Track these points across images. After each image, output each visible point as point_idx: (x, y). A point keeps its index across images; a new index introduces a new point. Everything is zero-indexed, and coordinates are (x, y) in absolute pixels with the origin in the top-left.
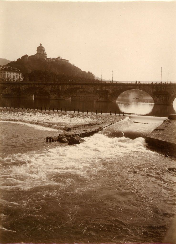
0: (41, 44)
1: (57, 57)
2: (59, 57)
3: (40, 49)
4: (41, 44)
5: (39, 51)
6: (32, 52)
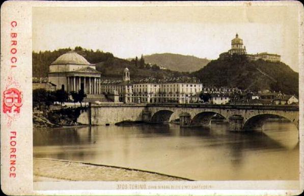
0: (237, 35)
3: (236, 42)
4: (237, 35)
6: (227, 48)
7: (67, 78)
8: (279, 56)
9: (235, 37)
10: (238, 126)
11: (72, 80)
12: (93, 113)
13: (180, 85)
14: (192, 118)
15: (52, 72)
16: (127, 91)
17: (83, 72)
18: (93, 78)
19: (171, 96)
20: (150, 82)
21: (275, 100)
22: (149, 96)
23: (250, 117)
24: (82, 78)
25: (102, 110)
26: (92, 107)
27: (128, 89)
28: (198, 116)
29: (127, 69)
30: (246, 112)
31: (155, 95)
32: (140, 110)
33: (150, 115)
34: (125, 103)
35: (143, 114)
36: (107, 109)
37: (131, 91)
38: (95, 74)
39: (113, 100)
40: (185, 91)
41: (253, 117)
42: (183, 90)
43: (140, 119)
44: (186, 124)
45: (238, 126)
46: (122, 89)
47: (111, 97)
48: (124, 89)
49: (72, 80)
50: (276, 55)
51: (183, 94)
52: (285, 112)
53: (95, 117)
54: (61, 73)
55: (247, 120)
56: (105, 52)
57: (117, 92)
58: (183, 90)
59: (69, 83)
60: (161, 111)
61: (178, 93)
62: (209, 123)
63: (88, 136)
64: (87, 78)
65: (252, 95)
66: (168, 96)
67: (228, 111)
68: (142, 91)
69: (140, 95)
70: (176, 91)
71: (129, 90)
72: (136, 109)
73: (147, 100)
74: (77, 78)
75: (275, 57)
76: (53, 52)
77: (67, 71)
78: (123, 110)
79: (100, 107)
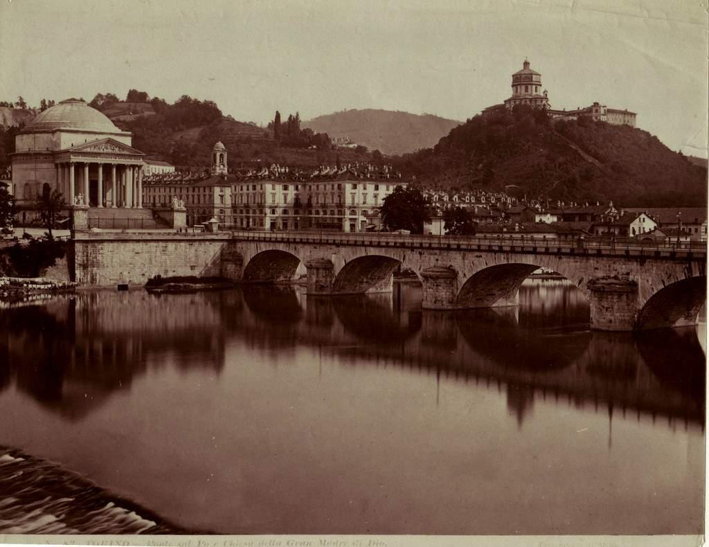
0: (526, 64)
1: (590, 104)
2: (596, 104)
3: (523, 79)
4: (526, 64)
5: (519, 87)
6: (501, 93)
7: (56, 166)
8: (633, 115)
9: (522, 67)
10: (443, 293)
11: (66, 170)
12: (79, 259)
13: (268, 187)
14: (337, 270)
15: (20, 151)
16: (217, 201)
17: (96, 151)
18: (121, 168)
19: (325, 213)
20: (271, 178)
21: (598, 225)
22: (268, 211)
23: (479, 270)
24: (94, 167)
25: (107, 247)
26: (79, 241)
27: (222, 196)
28: (350, 267)
29: (220, 145)
30: (463, 259)
31: (285, 212)
32: (214, 250)
33: (238, 260)
34: (208, 229)
35: (223, 258)
36: (122, 246)
37: (228, 201)
38: (130, 156)
39: (169, 224)
40: (359, 200)
41: (482, 271)
42: (353, 199)
43: (215, 272)
44: (322, 288)
45: (443, 293)
46: (199, 196)
47: (166, 216)
48: (211, 196)
49: (66, 170)
50: (625, 113)
51: (353, 210)
52: (560, 258)
53: (85, 267)
54: (40, 154)
55: (465, 280)
56: (201, 100)
57: (182, 203)
58: (353, 199)
59: (60, 181)
60: (267, 252)
61: (341, 205)
62: (386, 284)
63: (562, 304)
64: (108, 168)
65: (537, 212)
66: (317, 213)
67: (420, 254)
68: (157, 201)
69: (248, 212)
70: (336, 200)
71: (223, 197)
72: (202, 248)
73: (262, 224)
74: (79, 167)
75: (621, 117)
76: (177, 105)
77: (57, 150)
78: (164, 250)
79: (102, 241)
